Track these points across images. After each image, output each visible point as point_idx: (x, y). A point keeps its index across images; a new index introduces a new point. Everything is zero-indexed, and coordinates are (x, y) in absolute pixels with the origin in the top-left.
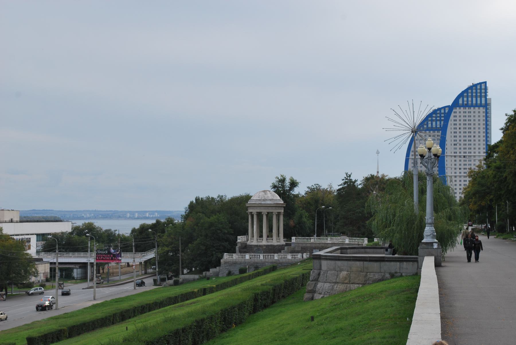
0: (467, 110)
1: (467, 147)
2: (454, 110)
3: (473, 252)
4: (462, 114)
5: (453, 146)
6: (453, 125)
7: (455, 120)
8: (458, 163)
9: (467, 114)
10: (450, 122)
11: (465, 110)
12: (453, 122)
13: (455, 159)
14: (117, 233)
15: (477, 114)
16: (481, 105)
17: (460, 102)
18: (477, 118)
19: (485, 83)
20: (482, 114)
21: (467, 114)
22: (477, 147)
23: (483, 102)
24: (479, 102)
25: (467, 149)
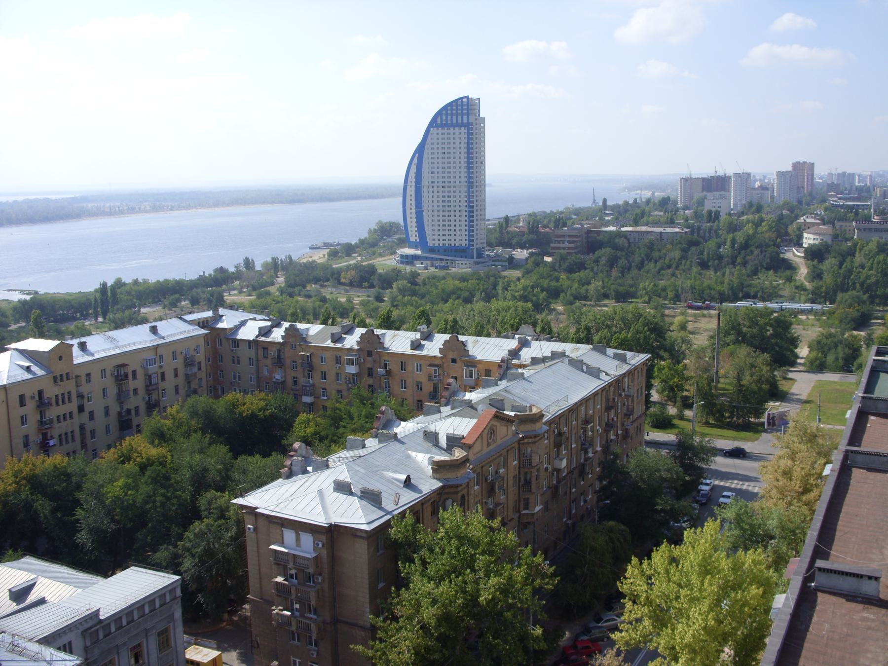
0: (446, 131)
1: (446, 175)
4: (458, 238)
5: (430, 175)
9: (446, 136)
12: (430, 146)
14: (207, 275)
15: (457, 136)
16: (462, 125)
17: (439, 121)
18: (458, 223)
20: (463, 136)
22: (457, 175)
23: (465, 121)
24: (460, 121)
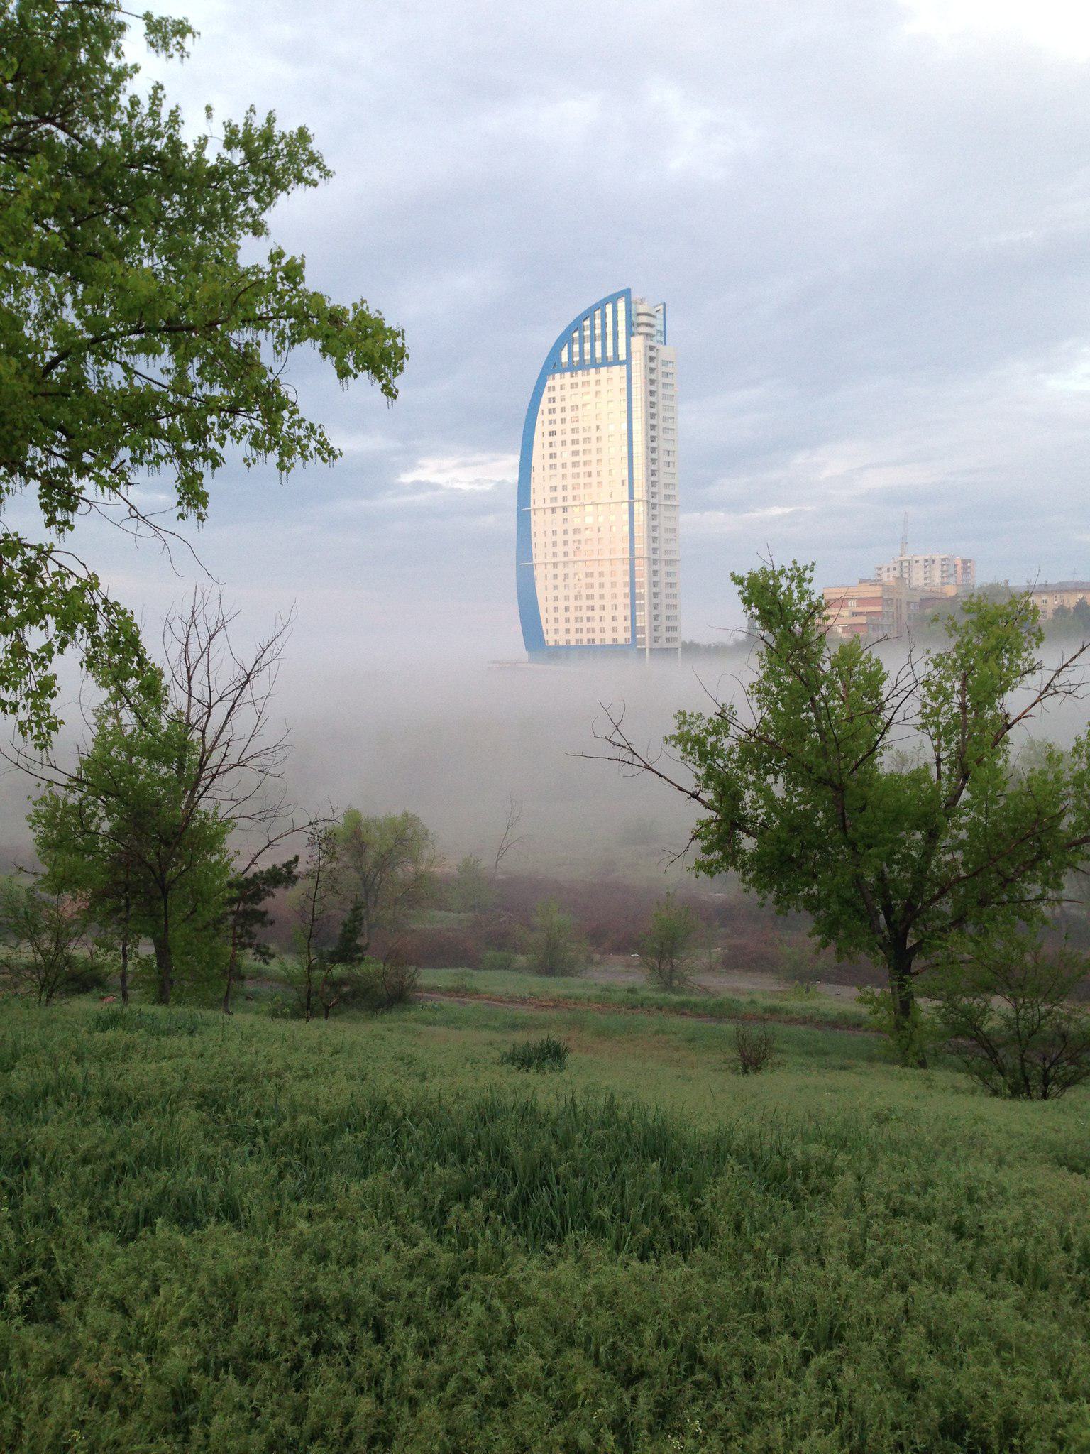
2: (550, 383)
6: (546, 423)
7: (552, 422)
10: (540, 418)
11: (574, 380)
17: (565, 358)
19: (626, 293)
22: (608, 614)
25: (584, 608)
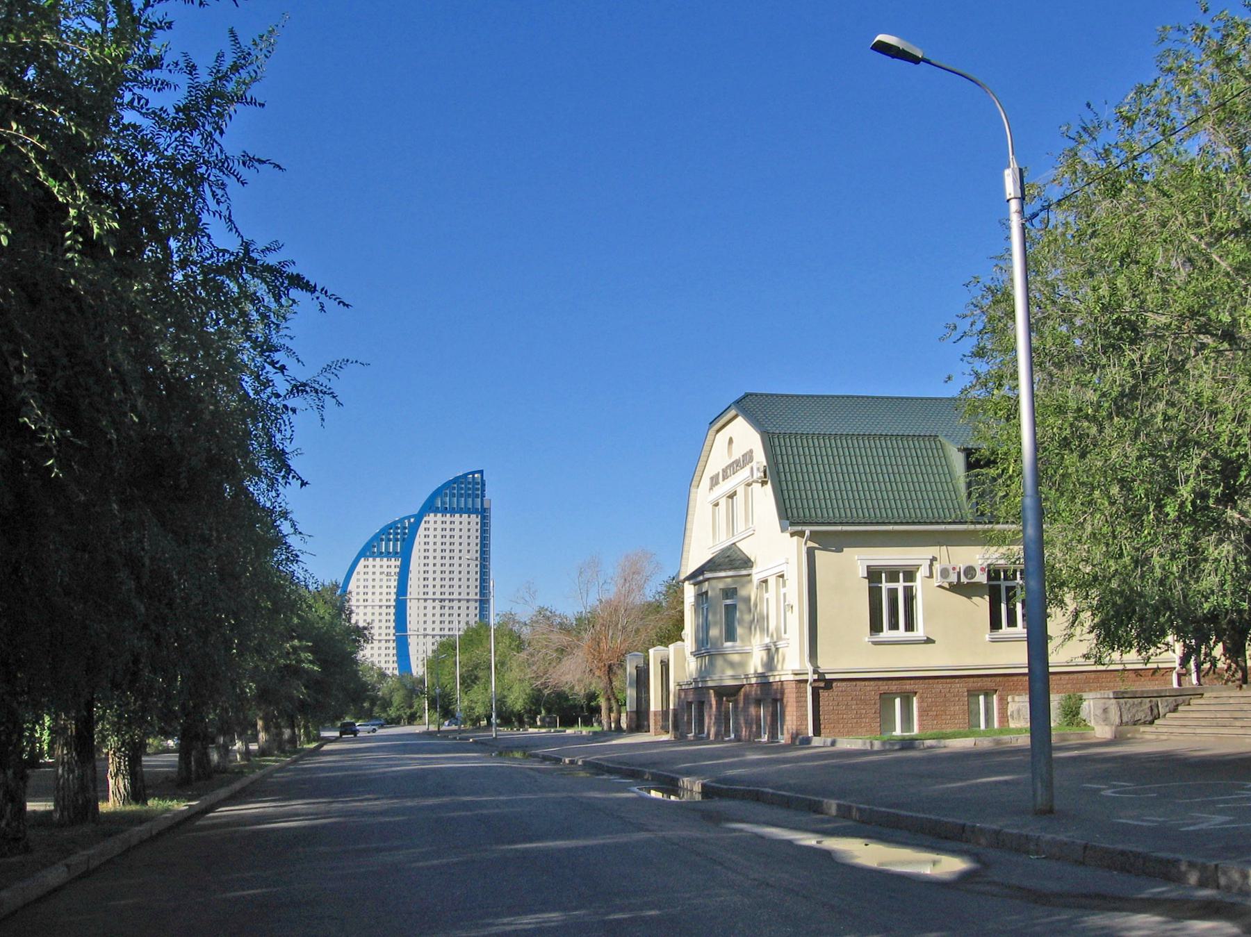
0: (448, 518)
3: (950, 865)
8: (430, 611)
13: (451, 604)
15: (457, 526)
16: (476, 511)
19: (481, 472)
21: (448, 526)
